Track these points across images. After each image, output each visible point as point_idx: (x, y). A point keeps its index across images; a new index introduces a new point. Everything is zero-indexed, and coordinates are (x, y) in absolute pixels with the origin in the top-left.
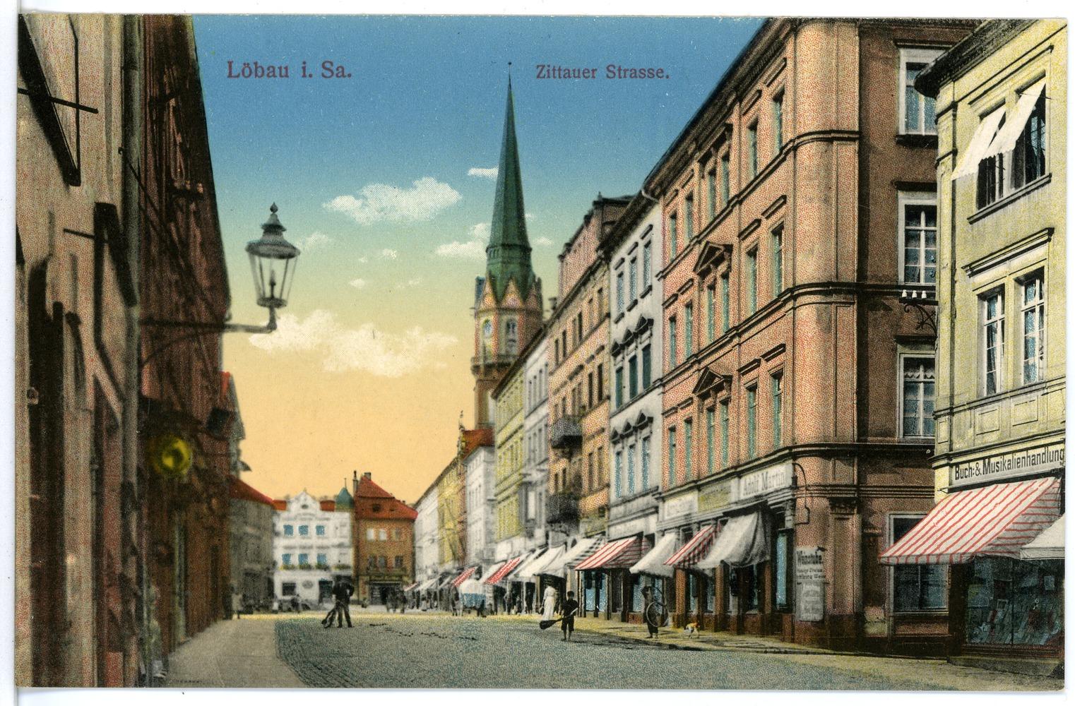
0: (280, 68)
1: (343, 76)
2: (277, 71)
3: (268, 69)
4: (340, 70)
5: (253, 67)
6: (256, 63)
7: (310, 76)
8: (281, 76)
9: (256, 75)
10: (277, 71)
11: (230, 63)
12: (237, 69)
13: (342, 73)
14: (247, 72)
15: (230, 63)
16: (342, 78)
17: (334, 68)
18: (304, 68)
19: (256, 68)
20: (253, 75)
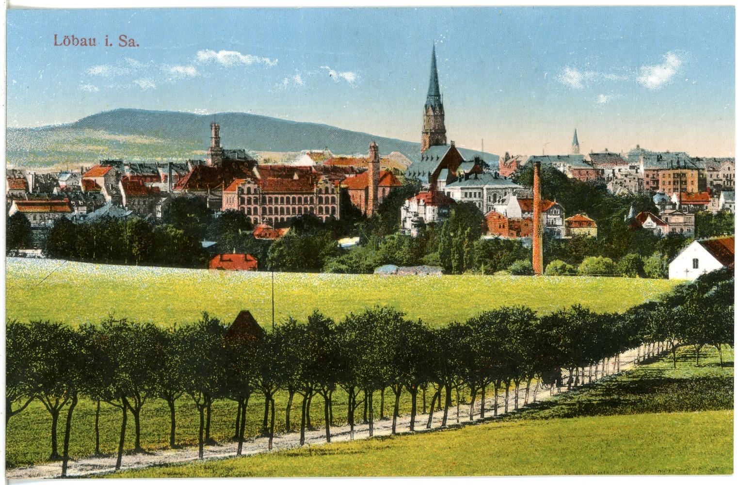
0: (90, 40)
1: (134, 46)
2: (88, 42)
3: (82, 40)
6: (73, 36)
7: (138, 45)
12: (60, 40)
13: (132, 43)
14: (67, 42)
17: (127, 40)
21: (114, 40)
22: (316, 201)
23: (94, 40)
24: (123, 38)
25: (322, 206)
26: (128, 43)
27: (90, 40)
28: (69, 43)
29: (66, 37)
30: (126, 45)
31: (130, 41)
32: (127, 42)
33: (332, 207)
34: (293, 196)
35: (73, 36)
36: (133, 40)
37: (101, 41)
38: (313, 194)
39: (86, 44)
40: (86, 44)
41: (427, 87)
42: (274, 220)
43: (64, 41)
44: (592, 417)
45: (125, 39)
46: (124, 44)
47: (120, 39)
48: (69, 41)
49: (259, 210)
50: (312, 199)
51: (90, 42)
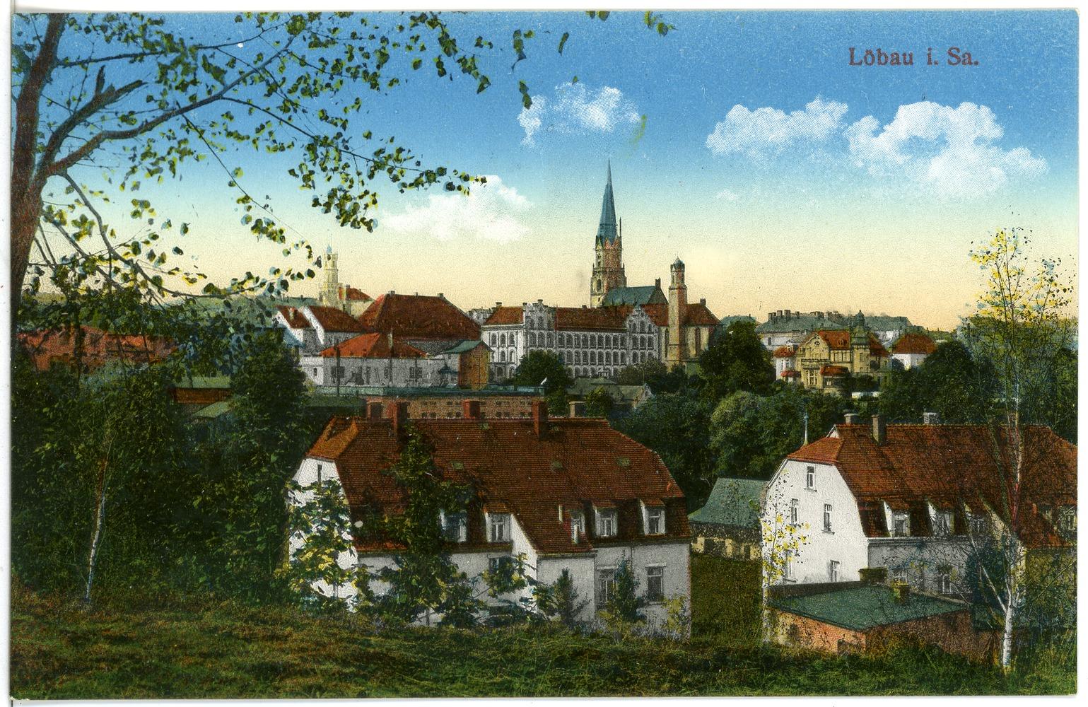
2: (901, 60)
5: (875, 52)
6: (879, 50)
10: (901, 57)
11: (852, 50)
12: (859, 55)
14: (869, 60)
15: (852, 50)
17: (960, 55)
22: (629, 343)
23: (911, 56)
24: (954, 51)
25: (595, 350)
26: (962, 59)
27: (904, 55)
28: (873, 61)
29: (869, 52)
30: (956, 64)
31: (964, 56)
32: (959, 57)
33: (599, 353)
34: (591, 333)
36: (951, 49)
38: (625, 331)
39: (898, 63)
40: (898, 63)
41: (600, 215)
42: (647, 355)
43: (865, 58)
44: (863, 533)
45: (957, 54)
46: (954, 60)
47: (951, 54)
48: (873, 56)
49: (654, 341)
50: (623, 340)
51: (905, 58)
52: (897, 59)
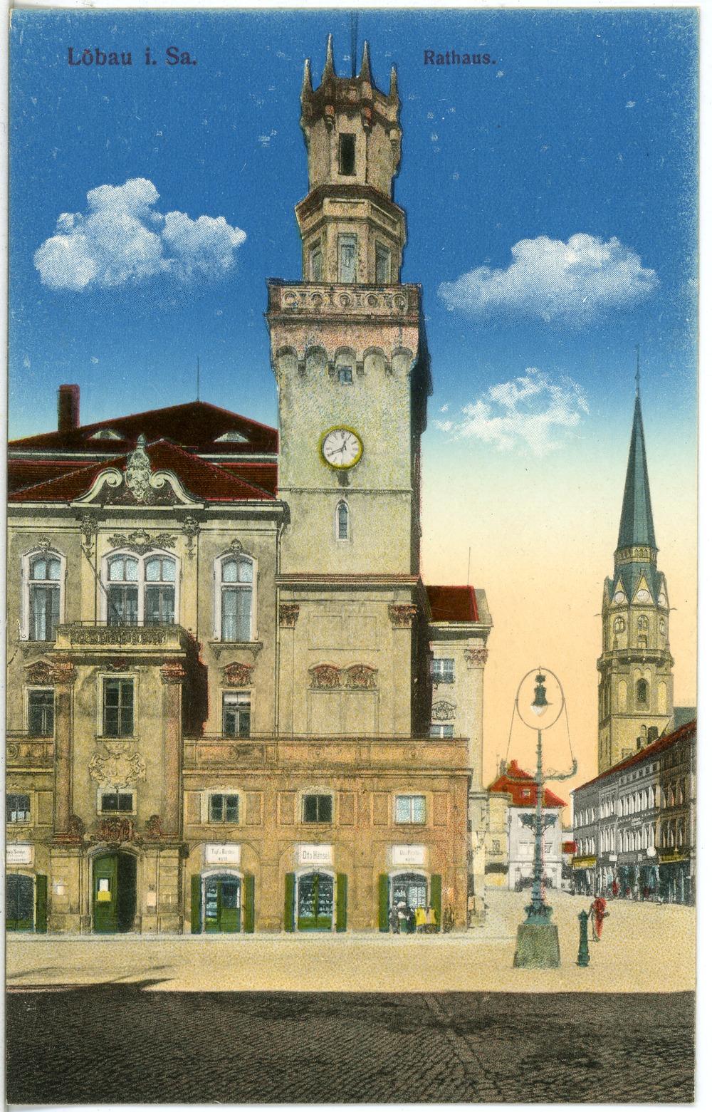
0: (123, 55)
1: (188, 62)
2: (120, 59)
4: (185, 56)
5: (94, 53)
8: (124, 63)
9: (98, 62)
11: (71, 50)
12: (77, 56)
13: (187, 60)
16: (114, 66)
17: (178, 54)
18: (148, 55)
19: (98, 54)
20: (471, 57)
21: (138, 57)
23: (129, 55)
24: (173, 51)
26: (180, 59)
27: (123, 55)
28: (92, 60)
30: (176, 63)
35: (97, 50)
37: (138, 57)
39: (117, 63)
46: (173, 60)
52: (116, 59)
